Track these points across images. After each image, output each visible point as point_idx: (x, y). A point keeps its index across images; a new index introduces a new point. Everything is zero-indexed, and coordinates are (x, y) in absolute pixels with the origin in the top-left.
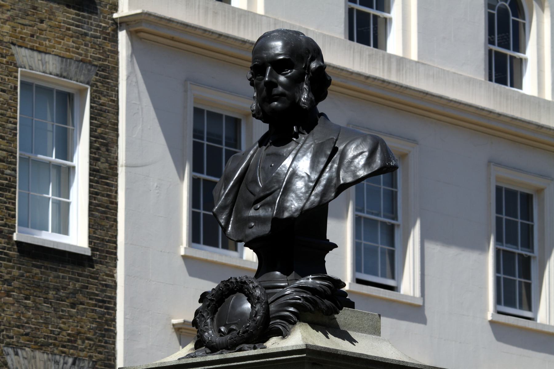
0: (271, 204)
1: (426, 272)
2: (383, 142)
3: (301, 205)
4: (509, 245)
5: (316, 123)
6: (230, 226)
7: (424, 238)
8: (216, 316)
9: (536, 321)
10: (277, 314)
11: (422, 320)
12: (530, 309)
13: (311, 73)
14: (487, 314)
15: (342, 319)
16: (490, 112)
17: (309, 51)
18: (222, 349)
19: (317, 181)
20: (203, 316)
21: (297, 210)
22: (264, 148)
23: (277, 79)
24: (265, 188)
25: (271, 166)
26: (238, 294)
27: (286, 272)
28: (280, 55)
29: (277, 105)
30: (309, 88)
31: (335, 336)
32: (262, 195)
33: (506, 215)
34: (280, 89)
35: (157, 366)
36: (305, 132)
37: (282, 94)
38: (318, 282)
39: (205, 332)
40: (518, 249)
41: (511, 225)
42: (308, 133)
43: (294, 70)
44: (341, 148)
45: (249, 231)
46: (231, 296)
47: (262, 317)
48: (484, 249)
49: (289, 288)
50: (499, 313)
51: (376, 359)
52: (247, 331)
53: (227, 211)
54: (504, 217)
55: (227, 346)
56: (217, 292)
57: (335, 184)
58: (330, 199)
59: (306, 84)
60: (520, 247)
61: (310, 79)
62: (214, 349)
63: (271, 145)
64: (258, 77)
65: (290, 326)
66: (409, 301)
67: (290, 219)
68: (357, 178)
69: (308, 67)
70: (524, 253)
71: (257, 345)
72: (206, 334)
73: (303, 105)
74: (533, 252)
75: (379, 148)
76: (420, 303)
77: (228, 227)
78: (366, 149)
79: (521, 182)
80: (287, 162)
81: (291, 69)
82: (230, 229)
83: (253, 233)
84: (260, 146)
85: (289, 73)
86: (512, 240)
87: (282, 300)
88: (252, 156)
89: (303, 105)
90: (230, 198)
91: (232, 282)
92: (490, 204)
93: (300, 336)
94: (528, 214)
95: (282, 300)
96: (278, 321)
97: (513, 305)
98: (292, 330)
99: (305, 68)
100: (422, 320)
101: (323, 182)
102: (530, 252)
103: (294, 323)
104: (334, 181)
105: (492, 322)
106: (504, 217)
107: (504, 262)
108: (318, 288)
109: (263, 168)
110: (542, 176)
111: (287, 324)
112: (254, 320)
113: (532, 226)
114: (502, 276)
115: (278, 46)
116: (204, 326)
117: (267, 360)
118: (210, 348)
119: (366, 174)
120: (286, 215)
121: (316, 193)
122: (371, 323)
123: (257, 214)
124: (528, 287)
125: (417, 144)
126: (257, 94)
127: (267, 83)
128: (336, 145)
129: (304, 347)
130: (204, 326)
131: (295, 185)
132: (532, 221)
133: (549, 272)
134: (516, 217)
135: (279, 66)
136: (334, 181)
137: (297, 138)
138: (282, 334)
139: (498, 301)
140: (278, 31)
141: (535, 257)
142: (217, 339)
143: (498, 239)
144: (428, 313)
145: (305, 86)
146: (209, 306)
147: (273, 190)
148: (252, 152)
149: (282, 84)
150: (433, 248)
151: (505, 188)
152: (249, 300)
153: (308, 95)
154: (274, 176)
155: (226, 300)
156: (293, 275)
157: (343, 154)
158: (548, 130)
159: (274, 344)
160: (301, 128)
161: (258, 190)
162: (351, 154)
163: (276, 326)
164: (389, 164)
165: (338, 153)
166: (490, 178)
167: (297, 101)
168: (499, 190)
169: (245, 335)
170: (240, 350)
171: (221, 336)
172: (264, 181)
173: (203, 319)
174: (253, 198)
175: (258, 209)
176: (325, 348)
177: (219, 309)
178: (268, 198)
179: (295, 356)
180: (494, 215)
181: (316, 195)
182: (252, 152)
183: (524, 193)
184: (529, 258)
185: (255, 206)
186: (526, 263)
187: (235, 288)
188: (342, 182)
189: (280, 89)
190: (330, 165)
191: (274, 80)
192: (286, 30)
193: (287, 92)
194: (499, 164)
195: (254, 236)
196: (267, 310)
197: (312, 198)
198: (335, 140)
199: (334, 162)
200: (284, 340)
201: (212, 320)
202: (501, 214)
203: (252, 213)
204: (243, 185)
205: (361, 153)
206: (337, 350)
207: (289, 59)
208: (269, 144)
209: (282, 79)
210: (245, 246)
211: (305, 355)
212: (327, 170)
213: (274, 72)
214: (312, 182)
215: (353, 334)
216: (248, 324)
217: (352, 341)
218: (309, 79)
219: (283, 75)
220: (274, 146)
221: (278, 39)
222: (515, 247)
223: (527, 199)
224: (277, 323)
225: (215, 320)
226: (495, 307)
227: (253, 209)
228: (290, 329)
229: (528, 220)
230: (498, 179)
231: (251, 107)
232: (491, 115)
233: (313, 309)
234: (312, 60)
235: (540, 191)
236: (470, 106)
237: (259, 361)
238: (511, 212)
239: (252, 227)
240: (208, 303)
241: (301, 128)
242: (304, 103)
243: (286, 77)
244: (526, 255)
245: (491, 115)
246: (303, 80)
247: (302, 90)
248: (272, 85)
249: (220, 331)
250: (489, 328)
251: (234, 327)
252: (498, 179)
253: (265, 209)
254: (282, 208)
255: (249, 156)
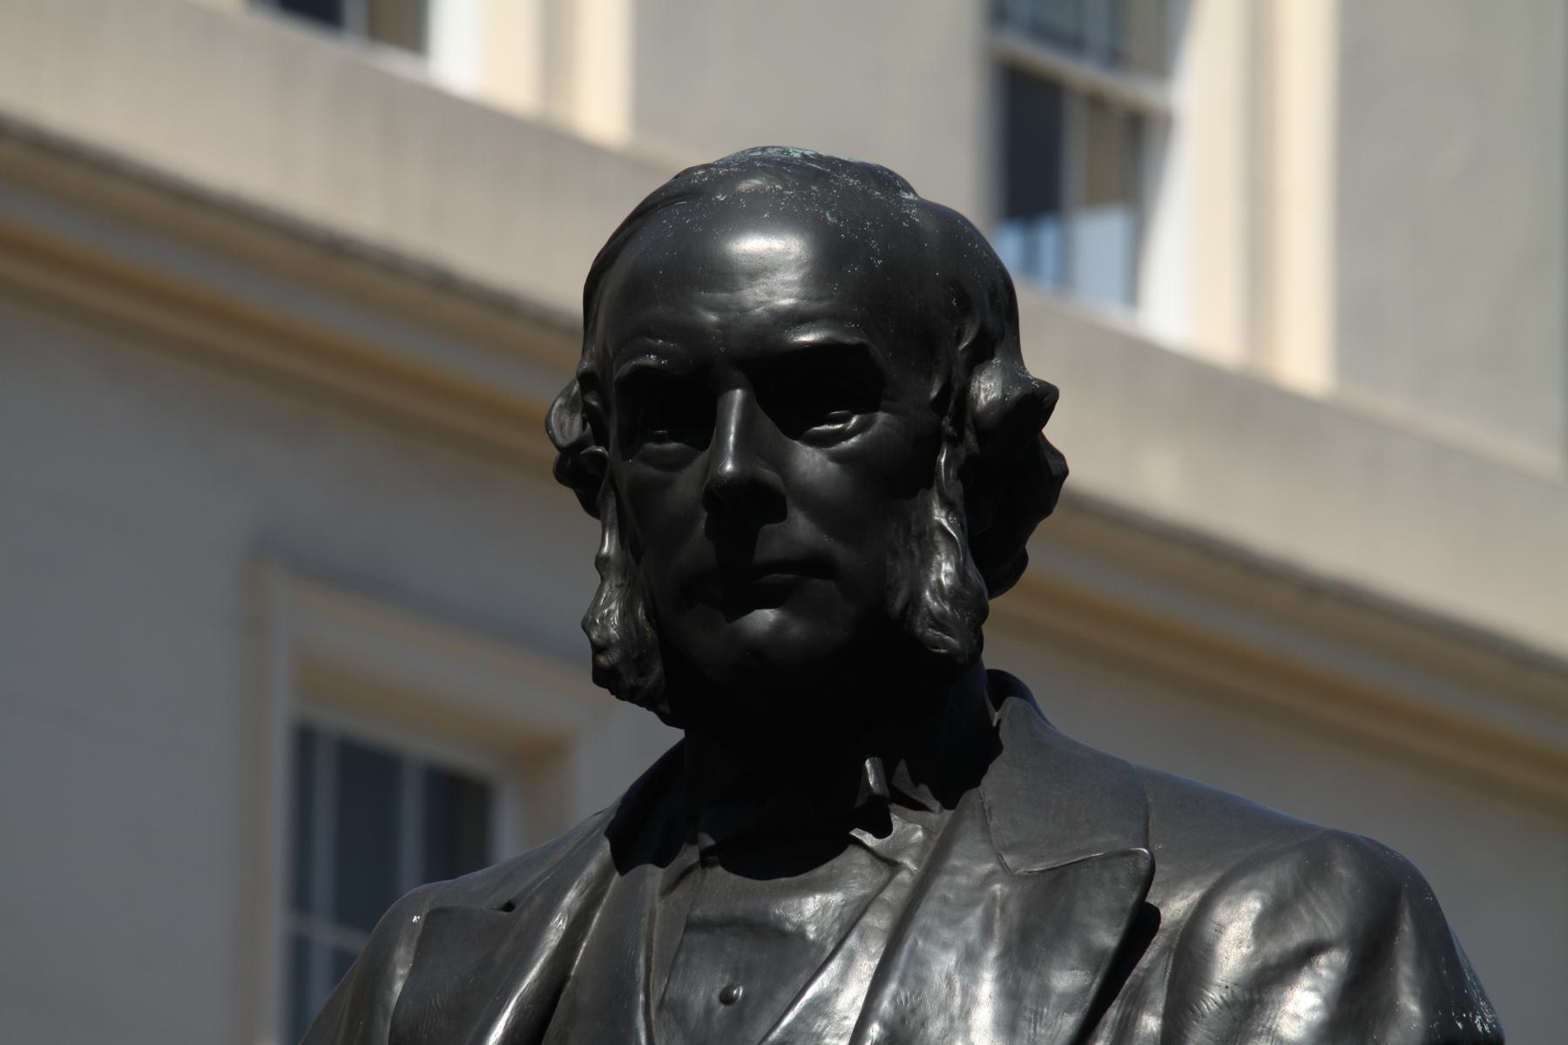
2: (1421, 889)
5: (986, 747)
13: (970, 437)
22: (654, 876)
23: (781, 464)
25: (726, 998)
28: (797, 318)
29: (778, 627)
30: (961, 528)
34: (801, 528)
36: (924, 794)
37: (815, 565)
42: (949, 802)
43: (881, 417)
44: (1175, 908)
59: (948, 505)
61: (967, 472)
63: (706, 860)
64: (652, 446)
69: (957, 398)
73: (931, 633)
75: (1406, 927)
81: (866, 404)
84: (623, 859)
85: (855, 432)
88: (578, 925)
89: (931, 633)
99: (939, 405)
115: (772, 261)
126: (624, 540)
127: (719, 496)
128: (1151, 900)
135: (796, 384)
137: (882, 830)
145: (940, 516)
148: (571, 898)
153: (961, 573)
160: (902, 768)
162: (1234, 942)
164: (1470, 1025)
165: (1159, 941)
167: (899, 604)
180: (275, 921)
182: (571, 898)
189: (801, 528)
190: (1113, 1014)
191: (769, 475)
192: (819, 159)
193: (842, 553)
198: (1143, 866)
199: (1138, 1002)
205: (1305, 956)
207: (859, 349)
208: (689, 855)
209: (810, 462)
213: (766, 424)
218: (963, 474)
231: (587, 626)
234: (980, 356)
241: (902, 768)
242: (939, 622)
243: (838, 458)
246: (927, 475)
248: (753, 502)
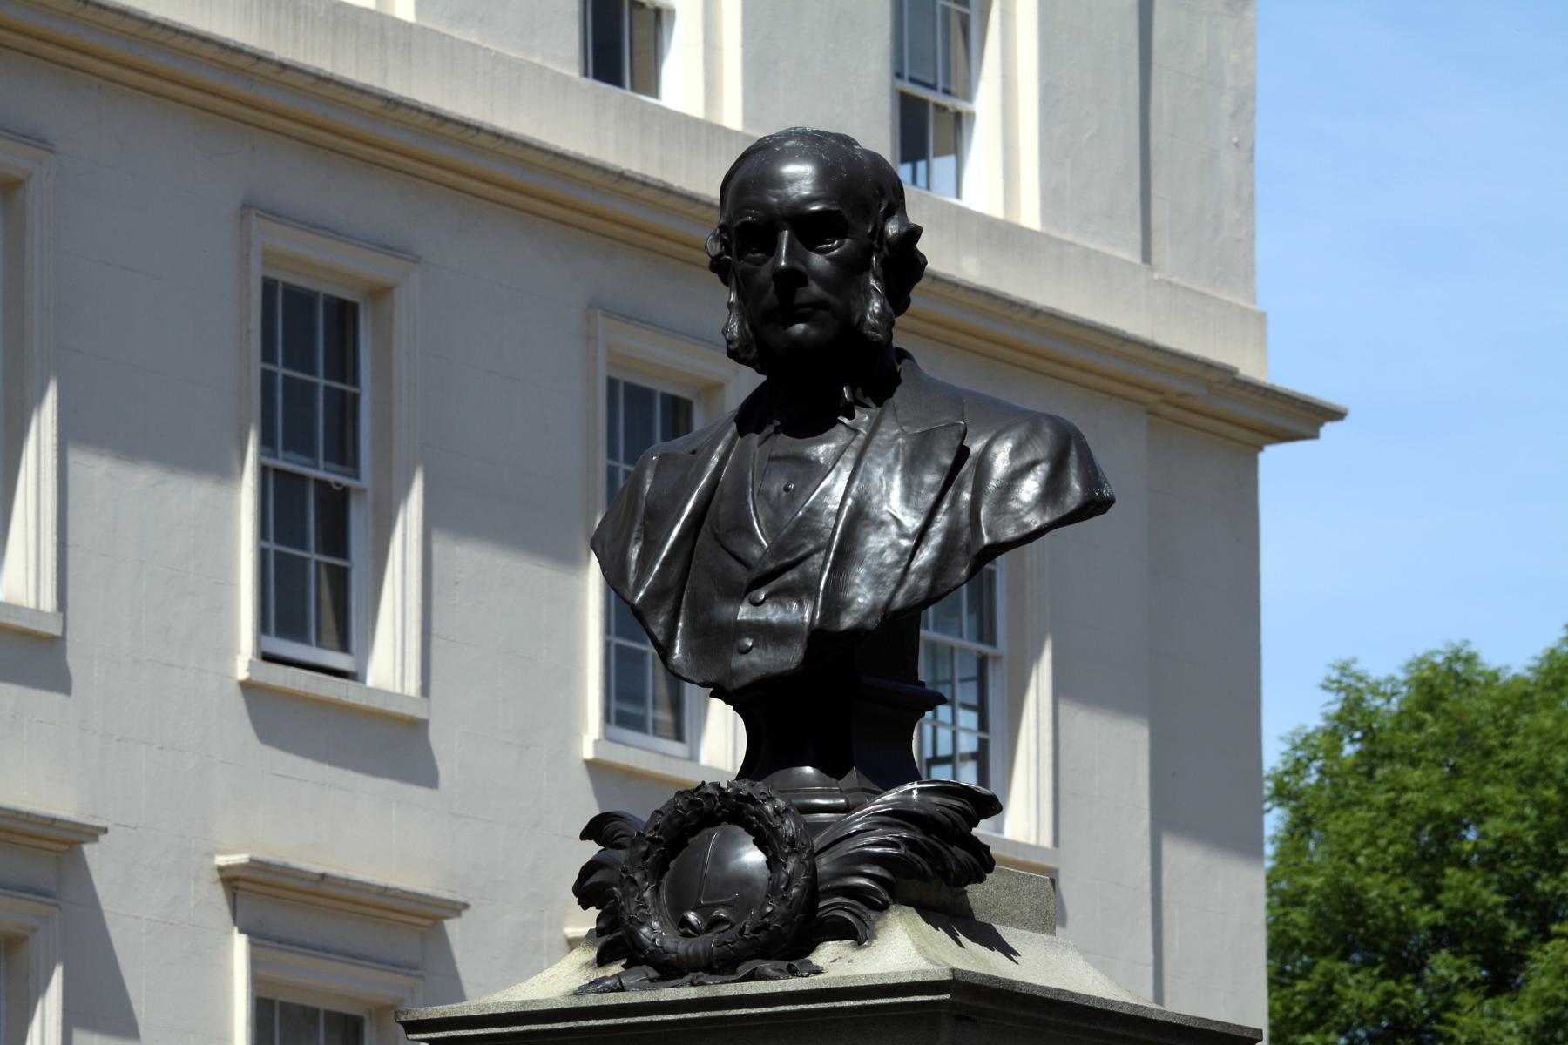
0: (802, 591)
1: (72, 539)
2: (1079, 436)
3: (885, 597)
4: (292, 455)
5: (895, 380)
6: (678, 642)
7: (67, 437)
8: (665, 881)
9: (364, 681)
10: (838, 883)
11: (60, 681)
12: (344, 646)
14: (235, 660)
15: (978, 894)
16: (259, 58)
17: (881, 190)
18: (694, 970)
19: (921, 536)
20: (634, 882)
21: (873, 610)
22: (755, 438)
23: (805, 262)
24: (778, 549)
25: (786, 489)
26: (725, 826)
27: (833, 768)
28: (810, 200)
29: (806, 332)
31: (974, 940)
32: (771, 566)
33: (326, 376)
34: (814, 289)
35: (512, 1010)
36: (869, 401)
37: (820, 304)
38: (935, 799)
39: (642, 924)
40: (316, 467)
41: (299, 395)
42: (879, 403)
44: (976, 447)
45: (739, 661)
46: (706, 831)
47: (803, 889)
48: (227, 473)
49: (866, 818)
50: (268, 658)
51: (1090, 1004)
52: (766, 926)
53: (668, 605)
54: (281, 371)
55: (711, 964)
56: (670, 819)
57: (968, 546)
58: (955, 583)
59: (877, 278)
60: (280, 452)
61: (884, 263)
62: (670, 970)
63: (777, 431)
65: (872, 914)
66: (25, 624)
67: (856, 632)
68: (1026, 531)
69: (880, 232)
70: (332, 478)
71: (795, 964)
72: (645, 930)
74: (356, 476)
75: (1074, 453)
76: (56, 631)
77: (674, 646)
78: (1040, 449)
79: (330, 266)
80: (836, 486)
81: (841, 235)
82: (677, 650)
83: (752, 665)
84: (742, 431)
85: (836, 248)
86: (300, 442)
87: (849, 847)
90: (676, 569)
91: (708, 795)
92: (249, 331)
93: (909, 943)
94: (344, 364)
95: (849, 847)
96: (838, 899)
97: (299, 635)
98: (879, 924)
100: (60, 681)
101: (935, 539)
102: (349, 476)
103: (883, 908)
104: (966, 536)
105: (247, 687)
106: (281, 371)
107: (282, 504)
108: (941, 818)
109: (764, 494)
110: (387, 249)
111: (865, 908)
112: (785, 899)
113: (356, 397)
114: (272, 547)
115: (800, 176)
116: (638, 908)
117: (838, 1004)
118: (656, 968)
119: (1047, 519)
120: (847, 621)
121: (920, 568)
122: (1036, 901)
123: (762, 618)
124: (339, 581)
125: (52, 151)
129: (947, 977)
130: (638, 908)
131: (863, 544)
132: (356, 383)
133: (404, 535)
134: (313, 372)
135: (811, 227)
136: (966, 536)
138: (857, 935)
139: (263, 627)
140: (801, 135)
141: (361, 491)
142: (677, 945)
143: (267, 441)
144: (74, 661)
145: (873, 283)
146: (646, 855)
147: (800, 554)
148: (720, 448)
149: (818, 277)
150: (93, 468)
151: (285, 284)
152: (761, 844)
153: (883, 307)
154: (802, 518)
155: (691, 840)
156: (853, 777)
157: (983, 466)
158: (414, 113)
159: (836, 963)
161: (756, 552)
162: (1001, 461)
163: (839, 913)
165: (969, 461)
166: (248, 255)
168: (269, 287)
169: (761, 936)
170: (751, 977)
171: (685, 935)
172: (771, 529)
173: (632, 889)
174: (742, 575)
175: (762, 602)
176: (967, 972)
177: (672, 864)
178: (790, 576)
179: (918, 998)
180: (256, 366)
181: (922, 571)
182: (720, 448)
183: (331, 297)
184: (345, 492)
185: (753, 593)
186: (336, 505)
187: (719, 810)
188: (986, 540)
189: (814, 289)
190: (950, 492)
191: (800, 267)
193: (832, 299)
194: (273, 214)
195: (755, 675)
196: (813, 870)
197: (911, 578)
199: (961, 487)
200: (863, 952)
201: (656, 890)
202: (274, 362)
203: (744, 613)
204: (704, 536)
205: (1031, 466)
206: (1013, 983)
208: (770, 429)
209: (818, 261)
210: (713, 695)
211: (947, 996)
212: (945, 506)
213: (798, 244)
214: (906, 536)
215: (1008, 934)
216: (769, 909)
217: (1008, 951)
219: (822, 252)
220: (788, 434)
221: (791, 156)
222: (308, 460)
223: (343, 315)
224: (834, 906)
225: (663, 892)
226: (258, 643)
227: (746, 601)
228: (873, 923)
229: (343, 381)
230: (268, 256)
231: (724, 332)
232: (261, 68)
233: (930, 872)
235: (381, 293)
236: (204, 39)
237: (811, 1006)
238: (300, 356)
239: (747, 651)
240: (644, 848)
242: (874, 328)
244: (338, 485)
245: (261, 68)
246: (867, 266)
247: (866, 294)
248: (793, 279)
249: (685, 922)
250: (238, 704)
251: (721, 913)
252: (268, 256)
253: (783, 605)
254: (835, 602)
255: (715, 459)
